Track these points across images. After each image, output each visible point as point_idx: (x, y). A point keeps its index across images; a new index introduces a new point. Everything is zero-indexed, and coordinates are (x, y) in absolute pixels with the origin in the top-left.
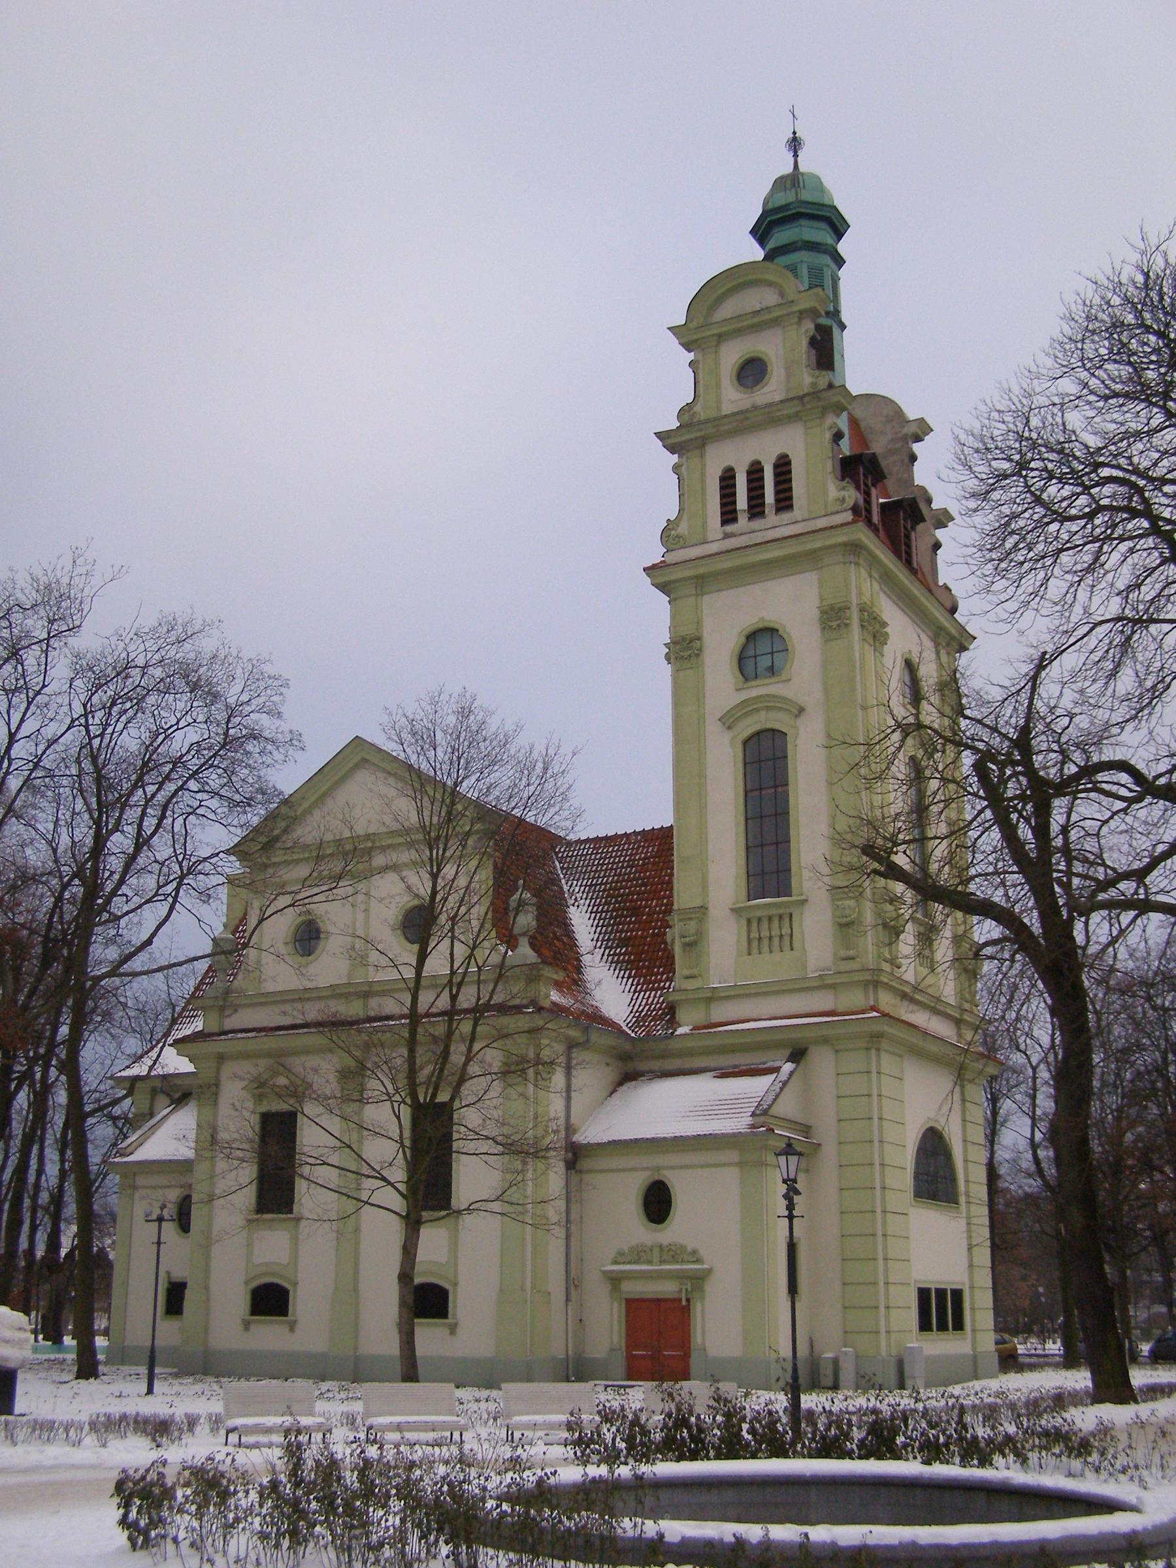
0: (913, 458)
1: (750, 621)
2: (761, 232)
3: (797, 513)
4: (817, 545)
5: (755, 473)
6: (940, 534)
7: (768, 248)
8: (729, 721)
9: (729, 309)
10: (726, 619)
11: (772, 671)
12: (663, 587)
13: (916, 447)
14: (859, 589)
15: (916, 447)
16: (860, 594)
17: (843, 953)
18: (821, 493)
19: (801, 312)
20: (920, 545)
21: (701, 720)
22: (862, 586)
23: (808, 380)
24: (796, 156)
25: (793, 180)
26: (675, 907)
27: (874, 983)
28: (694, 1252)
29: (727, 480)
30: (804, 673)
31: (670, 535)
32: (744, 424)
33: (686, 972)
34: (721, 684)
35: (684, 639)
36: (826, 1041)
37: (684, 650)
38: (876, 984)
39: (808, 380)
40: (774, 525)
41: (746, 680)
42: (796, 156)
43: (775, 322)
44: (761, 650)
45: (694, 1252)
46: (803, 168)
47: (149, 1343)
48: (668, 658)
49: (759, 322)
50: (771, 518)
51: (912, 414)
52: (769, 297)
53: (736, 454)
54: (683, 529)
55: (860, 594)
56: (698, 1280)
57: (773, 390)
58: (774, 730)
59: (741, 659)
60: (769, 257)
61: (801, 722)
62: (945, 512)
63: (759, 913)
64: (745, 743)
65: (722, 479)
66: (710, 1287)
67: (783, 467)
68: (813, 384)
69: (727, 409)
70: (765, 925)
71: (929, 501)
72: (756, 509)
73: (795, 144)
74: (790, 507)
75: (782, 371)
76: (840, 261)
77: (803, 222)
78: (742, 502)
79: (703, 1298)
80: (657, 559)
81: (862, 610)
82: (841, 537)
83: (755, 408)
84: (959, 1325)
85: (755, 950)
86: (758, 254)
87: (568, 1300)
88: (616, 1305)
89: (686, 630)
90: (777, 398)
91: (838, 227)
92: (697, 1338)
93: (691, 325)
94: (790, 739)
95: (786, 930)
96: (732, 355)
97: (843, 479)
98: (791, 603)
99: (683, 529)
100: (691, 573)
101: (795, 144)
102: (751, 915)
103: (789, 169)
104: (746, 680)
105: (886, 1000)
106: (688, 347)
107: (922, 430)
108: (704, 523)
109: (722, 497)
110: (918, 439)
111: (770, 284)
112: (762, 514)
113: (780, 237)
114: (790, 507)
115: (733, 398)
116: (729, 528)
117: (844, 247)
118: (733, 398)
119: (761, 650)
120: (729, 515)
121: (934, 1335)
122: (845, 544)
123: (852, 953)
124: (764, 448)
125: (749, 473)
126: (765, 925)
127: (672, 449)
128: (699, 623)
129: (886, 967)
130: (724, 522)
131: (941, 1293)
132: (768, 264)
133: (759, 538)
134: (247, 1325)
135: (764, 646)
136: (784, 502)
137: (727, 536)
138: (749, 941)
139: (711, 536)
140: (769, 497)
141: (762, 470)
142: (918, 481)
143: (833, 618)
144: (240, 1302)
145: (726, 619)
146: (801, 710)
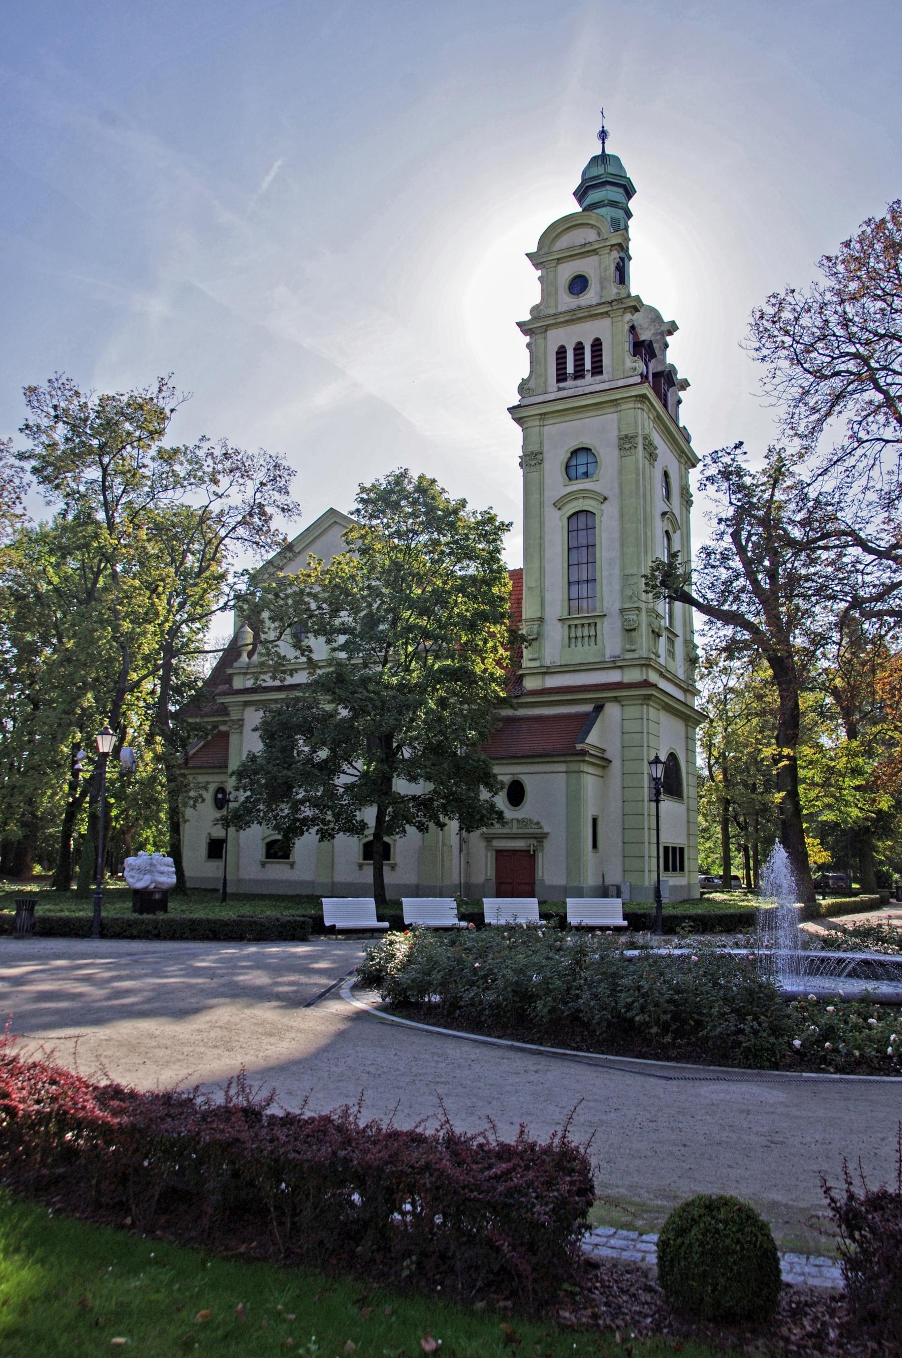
0: (666, 346)
1: (574, 444)
2: (580, 195)
3: (605, 376)
4: (619, 396)
5: (579, 349)
6: (682, 394)
7: (585, 205)
8: (559, 505)
9: (564, 242)
10: (561, 438)
11: (586, 475)
12: (519, 420)
13: (669, 339)
14: (643, 425)
15: (669, 339)
16: (643, 429)
17: (628, 647)
18: (620, 363)
19: (612, 246)
20: (671, 401)
21: (541, 505)
22: (642, 422)
23: (615, 291)
24: (603, 143)
25: (603, 158)
26: (524, 617)
27: (646, 664)
28: (538, 823)
29: (561, 353)
30: (605, 479)
31: (523, 389)
32: (574, 317)
33: (530, 657)
34: (556, 484)
35: (532, 453)
36: (616, 699)
37: (531, 460)
38: (648, 666)
39: (615, 291)
40: (589, 383)
41: (570, 480)
42: (603, 143)
43: (595, 252)
44: (580, 461)
45: (538, 823)
46: (607, 152)
47: (222, 876)
48: (521, 465)
49: (586, 251)
50: (588, 377)
51: (666, 319)
52: (591, 235)
53: (567, 336)
54: (532, 384)
55: (643, 429)
56: (541, 838)
57: (590, 297)
58: (587, 511)
59: (567, 467)
60: (584, 210)
61: (604, 506)
62: (686, 381)
63: (576, 622)
64: (569, 518)
65: (557, 353)
66: (547, 844)
67: (597, 345)
68: (618, 294)
69: (562, 308)
70: (580, 629)
71: (676, 373)
72: (579, 373)
73: (603, 135)
74: (601, 373)
75: (598, 286)
76: (629, 215)
77: (609, 187)
78: (570, 369)
79: (542, 850)
80: (516, 403)
81: (645, 438)
82: (634, 392)
83: (580, 308)
84: (682, 869)
85: (573, 645)
86: (577, 209)
87: (461, 851)
88: (489, 854)
89: (534, 448)
90: (594, 302)
91: (629, 192)
92: (539, 874)
93: (543, 252)
94: (597, 517)
95: (592, 633)
96: (567, 272)
97: (635, 356)
98: (599, 431)
99: (532, 384)
100: (538, 412)
101: (603, 135)
102: (571, 622)
103: (599, 152)
104: (570, 480)
105: (653, 677)
106: (537, 266)
107: (672, 328)
108: (546, 381)
109: (557, 364)
110: (670, 333)
111: (592, 226)
112: (583, 377)
113: (594, 196)
114: (601, 373)
115: (567, 301)
116: (561, 385)
117: (632, 205)
118: (567, 301)
119: (580, 461)
120: (562, 377)
121: (670, 873)
122: (636, 396)
123: (633, 647)
124: (586, 333)
125: (575, 349)
126: (580, 629)
127: (526, 332)
128: (541, 443)
129: (653, 656)
130: (558, 381)
131: (674, 849)
132: (586, 213)
133: (580, 391)
134: (263, 864)
135: (582, 459)
136: (597, 369)
137: (560, 389)
138: (570, 638)
139: (550, 389)
140: (588, 365)
141: (583, 348)
142: (669, 361)
143: (626, 442)
144: (203, 850)
145: (611, 641)
146: (605, 499)
